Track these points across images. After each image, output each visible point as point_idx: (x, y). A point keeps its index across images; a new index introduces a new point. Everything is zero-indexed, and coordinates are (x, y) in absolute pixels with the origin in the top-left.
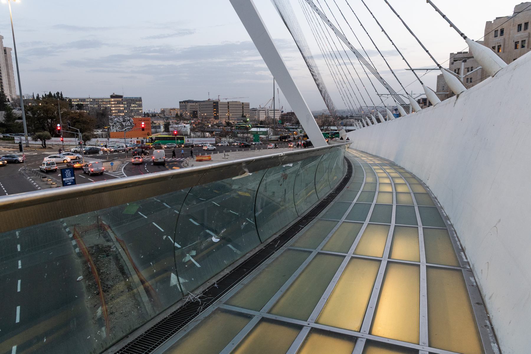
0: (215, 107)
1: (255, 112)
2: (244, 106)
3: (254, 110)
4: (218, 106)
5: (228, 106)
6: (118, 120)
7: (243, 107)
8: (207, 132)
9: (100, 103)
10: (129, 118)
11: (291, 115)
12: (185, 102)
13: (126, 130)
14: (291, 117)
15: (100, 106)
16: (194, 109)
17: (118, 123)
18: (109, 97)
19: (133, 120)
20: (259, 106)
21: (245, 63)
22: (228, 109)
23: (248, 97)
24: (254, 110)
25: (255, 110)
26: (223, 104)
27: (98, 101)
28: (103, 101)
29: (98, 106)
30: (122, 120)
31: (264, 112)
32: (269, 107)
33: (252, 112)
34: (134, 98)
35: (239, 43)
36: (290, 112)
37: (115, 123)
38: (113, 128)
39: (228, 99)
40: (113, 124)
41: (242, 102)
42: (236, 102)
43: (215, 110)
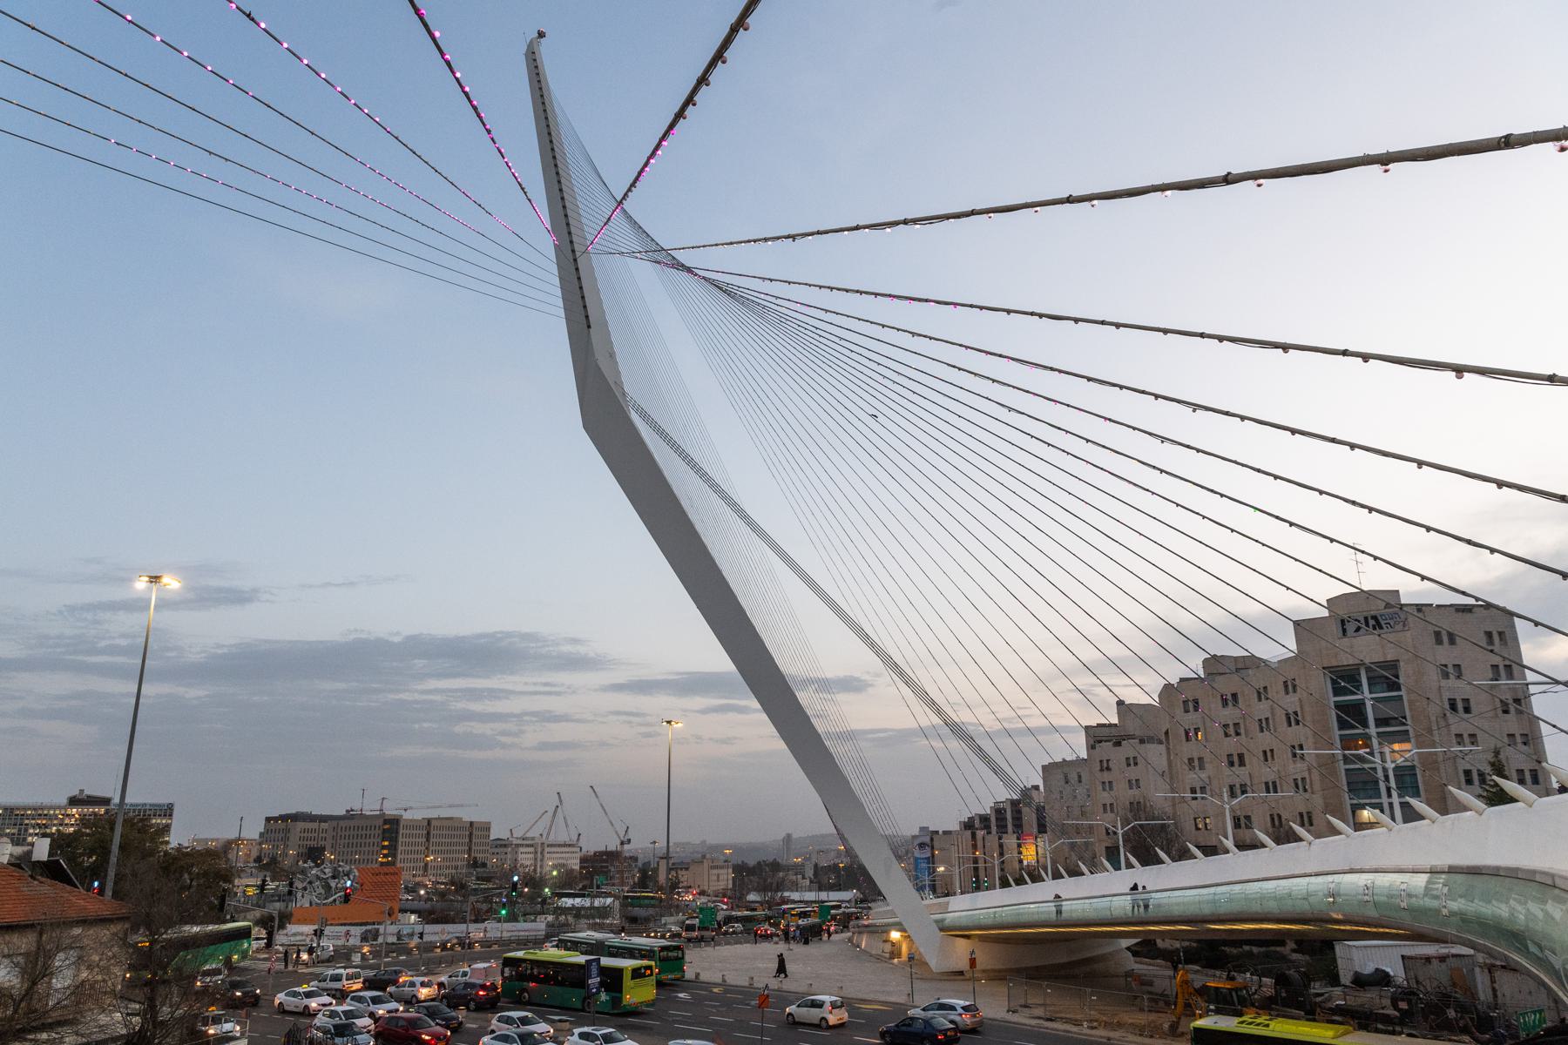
0: (387, 835)
1: (505, 850)
2: (474, 831)
3: (501, 846)
4: (397, 833)
5: (428, 833)
6: (319, 873)
7: (471, 834)
8: (413, 912)
9: (27, 822)
10: (347, 868)
11: (605, 861)
12: (284, 818)
13: (335, 900)
14: (607, 867)
15: (26, 830)
16: (312, 843)
17: (318, 883)
18: (64, 801)
19: (357, 874)
20: (509, 833)
21: (417, 697)
22: (428, 840)
23: (477, 805)
24: (501, 844)
25: (505, 846)
26: (414, 825)
27: (23, 815)
28: (40, 815)
29: (20, 830)
30: (330, 875)
31: (531, 849)
32: (541, 835)
33: (496, 850)
34: (148, 807)
35: (397, 639)
36: (603, 849)
37: (310, 883)
38: (303, 896)
39: (411, 808)
40: (305, 884)
41: (467, 819)
42: (451, 819)
43: (386, 843)
